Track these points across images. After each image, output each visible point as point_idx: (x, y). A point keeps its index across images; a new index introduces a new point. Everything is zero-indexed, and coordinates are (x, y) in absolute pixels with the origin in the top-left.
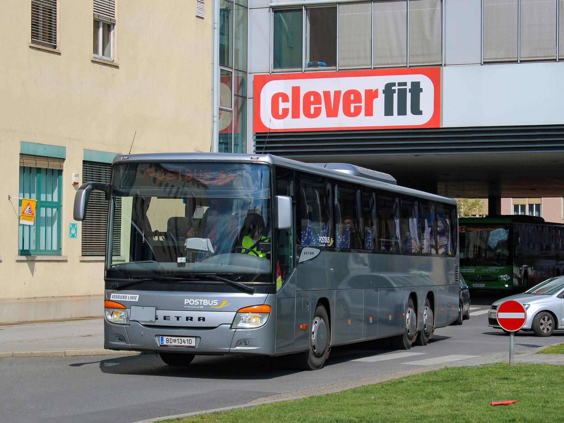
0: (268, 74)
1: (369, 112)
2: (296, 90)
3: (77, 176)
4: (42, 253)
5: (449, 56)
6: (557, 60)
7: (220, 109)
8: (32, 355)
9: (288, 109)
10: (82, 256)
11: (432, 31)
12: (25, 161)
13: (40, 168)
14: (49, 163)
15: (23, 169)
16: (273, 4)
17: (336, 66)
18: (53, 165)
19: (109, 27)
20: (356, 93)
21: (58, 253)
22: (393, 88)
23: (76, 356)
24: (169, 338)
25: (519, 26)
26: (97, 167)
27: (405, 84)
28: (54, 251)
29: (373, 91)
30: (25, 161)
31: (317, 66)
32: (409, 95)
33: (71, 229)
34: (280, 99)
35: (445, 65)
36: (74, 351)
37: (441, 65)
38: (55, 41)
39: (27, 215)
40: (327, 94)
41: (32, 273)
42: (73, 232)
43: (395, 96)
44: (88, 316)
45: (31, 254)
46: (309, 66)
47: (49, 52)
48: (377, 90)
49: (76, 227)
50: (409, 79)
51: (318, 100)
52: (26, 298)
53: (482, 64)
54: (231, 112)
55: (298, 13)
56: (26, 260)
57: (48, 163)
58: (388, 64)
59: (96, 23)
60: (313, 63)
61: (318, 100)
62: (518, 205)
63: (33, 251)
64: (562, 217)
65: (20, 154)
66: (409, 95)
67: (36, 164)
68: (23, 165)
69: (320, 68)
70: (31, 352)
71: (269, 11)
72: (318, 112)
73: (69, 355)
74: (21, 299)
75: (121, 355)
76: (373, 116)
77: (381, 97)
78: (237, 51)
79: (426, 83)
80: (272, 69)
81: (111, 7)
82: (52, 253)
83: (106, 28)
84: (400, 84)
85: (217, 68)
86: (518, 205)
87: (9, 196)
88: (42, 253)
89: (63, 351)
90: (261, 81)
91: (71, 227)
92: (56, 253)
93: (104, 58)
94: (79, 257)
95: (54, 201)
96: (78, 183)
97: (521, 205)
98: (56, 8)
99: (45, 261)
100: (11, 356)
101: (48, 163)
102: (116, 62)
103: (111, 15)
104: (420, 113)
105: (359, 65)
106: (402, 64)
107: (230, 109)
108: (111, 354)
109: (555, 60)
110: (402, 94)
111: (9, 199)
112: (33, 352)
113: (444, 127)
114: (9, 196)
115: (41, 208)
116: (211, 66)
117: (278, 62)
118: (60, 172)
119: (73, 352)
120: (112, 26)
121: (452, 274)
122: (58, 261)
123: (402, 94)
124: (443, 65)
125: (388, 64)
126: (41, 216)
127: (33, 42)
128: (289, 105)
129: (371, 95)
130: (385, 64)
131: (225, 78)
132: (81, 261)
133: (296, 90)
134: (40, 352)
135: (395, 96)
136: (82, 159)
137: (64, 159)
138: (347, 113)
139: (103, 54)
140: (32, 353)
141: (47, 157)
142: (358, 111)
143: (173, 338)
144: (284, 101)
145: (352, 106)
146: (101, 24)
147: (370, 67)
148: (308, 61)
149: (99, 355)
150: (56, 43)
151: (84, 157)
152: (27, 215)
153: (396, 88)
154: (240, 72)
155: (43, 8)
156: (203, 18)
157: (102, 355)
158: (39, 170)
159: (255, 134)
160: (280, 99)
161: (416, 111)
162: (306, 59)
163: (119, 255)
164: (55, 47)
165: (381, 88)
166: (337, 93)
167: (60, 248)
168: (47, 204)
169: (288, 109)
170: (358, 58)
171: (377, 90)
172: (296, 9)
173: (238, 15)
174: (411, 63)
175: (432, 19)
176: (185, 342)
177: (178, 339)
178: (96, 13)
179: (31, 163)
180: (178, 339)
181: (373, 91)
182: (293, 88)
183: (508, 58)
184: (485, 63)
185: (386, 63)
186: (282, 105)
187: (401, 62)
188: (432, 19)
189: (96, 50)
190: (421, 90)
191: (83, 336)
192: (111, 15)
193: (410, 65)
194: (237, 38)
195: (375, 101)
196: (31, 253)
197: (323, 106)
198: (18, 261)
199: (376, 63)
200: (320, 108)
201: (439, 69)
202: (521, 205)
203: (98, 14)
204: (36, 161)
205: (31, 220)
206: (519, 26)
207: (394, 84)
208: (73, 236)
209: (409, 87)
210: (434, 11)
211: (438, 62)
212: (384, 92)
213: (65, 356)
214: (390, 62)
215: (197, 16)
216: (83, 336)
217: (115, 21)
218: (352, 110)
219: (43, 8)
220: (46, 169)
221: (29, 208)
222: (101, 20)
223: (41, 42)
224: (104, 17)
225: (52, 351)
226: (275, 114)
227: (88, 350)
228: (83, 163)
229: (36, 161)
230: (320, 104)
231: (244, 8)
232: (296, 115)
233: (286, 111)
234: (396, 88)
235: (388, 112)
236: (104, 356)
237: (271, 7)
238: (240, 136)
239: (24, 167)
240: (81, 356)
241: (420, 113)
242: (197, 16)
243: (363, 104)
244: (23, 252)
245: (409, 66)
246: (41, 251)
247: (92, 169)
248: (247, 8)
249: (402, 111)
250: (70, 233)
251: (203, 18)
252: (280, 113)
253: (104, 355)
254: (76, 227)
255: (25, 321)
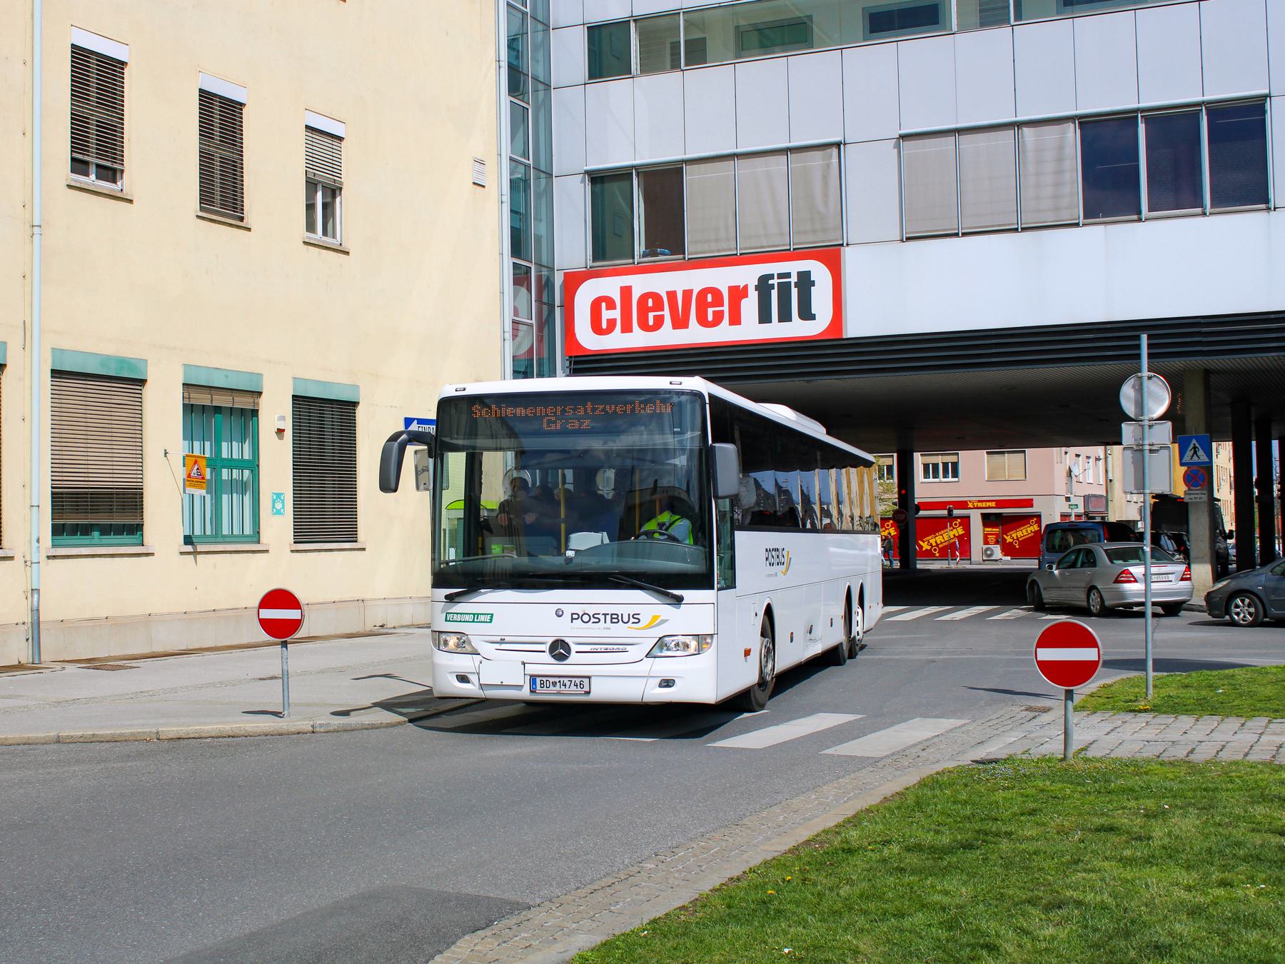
0: (584, 269)
1: (735, 320)
2: (626, 292)
3: (282, 418)
4: (226, 539)
5: (854, 231)
6: (1020, 230)
7: (514, 322)
8: (95, 739)
9: (615, 320)
10: (295, 542)
11: (826, 195)
12: (192, 395)
13: (221, 407)
14: (235, 398)
15: (189, 409)
16: (591, 167)
17: (684, 254)
18: (242, 402)
19: (333, 191)
20: (716, 293)
21: (255, 539)
22: (771, 282)
23: (179, 738)
24: (545, 679)
25: (959, 181)
26: (317, 406)
27: (788, 275)
28: (247, 536)
29: (741, 287)
30: (192, 395)
31: (656, 254)
32: (794, 292)
33: (274, 502)
34: (604, 305)
35: (847, 245)
36: (174, 729)
37: (842, 245)
38: (243, 210)
39: (195, 480)
40: (672, 295)
41: (1190, 624)
42: (279, 506)
43: (774, 293)
44: (307, 636)
45: (193, 542)
46: (645, 255)
47: (231, 225)
48: (746, 287)
49: (282, 498)
50: (794, 267)
51: (718, 299)
52: (200, 612)
53: (904, 240)
54: (531, 325)
55: (625, 184)
56: (192, 551)
57: (233, 399)
58: (762, 247)
59: (311, 185)
60: (651, 250)
61: (659, 305)
62: (948, 463)
63: (198, 537)
64: (986, 479)
65: (183, 384)
66: (794, 292)
67: (212, 401)
68: (190, 401)
69: (661, 257)
70: (92, 733)
71: (583, 181)
72: (659, 322)
73: (165, 737)
74: (190, 613)
75: (266, 736)
76: (729, 287)
77: (753, 295)
78: (538, 239)
79: (820, 273)
80: (590, 263)
81: (334, 162)
82: (242, 538)
83: (329, 192)
84: (781, 276)
85: (508, 261)
86: (948, 463)
87: (166, 450)
88: (226, 539)
89: (154, 730)
90: (574, 281)
91: (275, 498)
92: (249, 539)
93: (325, 238)
94: (291, 544)
95: (234, 457)
96: (284, 430)
97: (952, 463)
98: (242, 160)
99: (230, 552)
100: (55, 741)
101: (233, 399)
102: (345, 247)
103: (334, 174)
104: (813, 317)
105: (719, 251)
106: (783, 245)
107: (530, 322)
108: (247, 734)
109: (1016, 230)
110: (784, 290)
111: (166, 456)
112: (96, 733)
113: (849, 336)
114: (166, 450)
115: (223, 470)
116: (497, 257)
117: (600, 251)
118: (255, 413)
119: (173, 731)
120: (338, 192)
121: (680, 460)
122: (254, 552)
123: (784, 290)
124: (845, 245)
125: (762, 247)
126: (224, 478)
127: (202, 209)
128: (616, 314)
129: (738, 294)
130: (756, 248)
131: (521, 277)
132: (292, 551)
133: (626, 292)
134: (109, 732)
135: (774, 293)
136: (292, 393)
137: (260, 393)
138: (703, 321)
139: (325, 233)
140: (94, 734)
141: (232, 389)
142: (718, 318)
143: (552, 680)
144: (608, 308)
145: (710, 311)
146: (320, 187)
147: (735, 252)
148: (643, 248)
149: (224, 737)
150: (243, 214)
151: (294, 390)
152: (195, 480)
153: (775, 281)
154: (543, 269)
155: (221, 158)
156: (484, 186)
157: (229, 736)
158: (218, 409)
159: (567, 358)
160: (604, 305)
161: (806, 314)
162: (639, 246)
163: (356, 541)
164: (242, 219)
165: (752, 283)
166: (688, 294)
167: (257, 533)
168: (233, 464)
169: (615, 320)
170: (717, 240)
171: (746, 287)
172: (622, 175)
173: (537, 185)
174: (796, 244)
175: (825, 178)
176: (577, 685)
177: (560, 681)
178: (311, 170)
179: (202, 399)
180: (560, 681)
181: (741, 287)
182: (622, 288)
183: (944, 230)
184: (908, 239)
185: (759, 245)
186: (606, 315)
187: (781, 243)
188: (825, 178)
189: (311, 227)
190: (813, 283)
191: (260, 679)
192: (334, 174)
193: (795, 247)
194: (538, 219)
195: (744, 303)
196: (194, 540)
197: (666, 312)
198: (182, 553)
199: (744, 246)
200: (663, 316)
201: (839, 251)
202: (952, 463)
203: (314, 171)
204: (212, 395)
205: (202, 488)
206: (959, 181)
207: (771, 276)
208: (278, 512)
209: (794, 279)
210: (828, 166)
211: (836, 240)
212: (757, 288)
213: (158, 739)
214: (765, 244)
215: (474, 183)
216: (260, 679)
217: (341, 183)
218: (710, 318)
219: (221, 158)
220: (231, 408)
221: (197, 469)
222: (320, 182)
223: (218, 211)
224: (322, 176)
225: (133, 731)
226: (597, 328)
227: (203, 728)
228: (293, 400)
229: (212, 395)
230: (663, 310)
231: (548, 176)
232: (627, 328)
233: (612, 323)
234: (775, 281)
235: (765, 317)
236: (233, 739)
237: (587, 172)
238: (546, 362)
239: (192, 405)
240: (189, 738)
241: (813, 317)
242: (474, 183)
243: (726, 308)
244: (188, 540)
245: (794, 249)
246: (224, 536)
247: (310, 409)
248: (552, 175)
249: (785, 316)
250: (274, 507)
251: (484, 186)
252: (604, 326)
253: (233, 737)
254: (282, 498)
255: (198, 647)
